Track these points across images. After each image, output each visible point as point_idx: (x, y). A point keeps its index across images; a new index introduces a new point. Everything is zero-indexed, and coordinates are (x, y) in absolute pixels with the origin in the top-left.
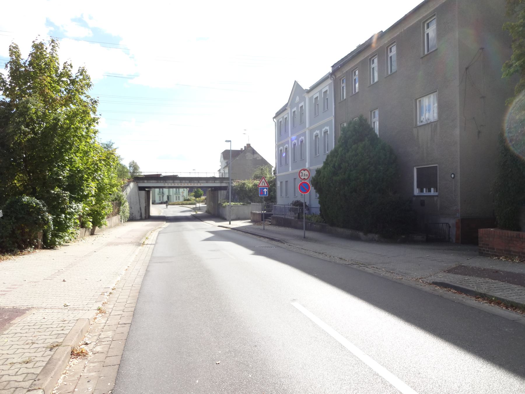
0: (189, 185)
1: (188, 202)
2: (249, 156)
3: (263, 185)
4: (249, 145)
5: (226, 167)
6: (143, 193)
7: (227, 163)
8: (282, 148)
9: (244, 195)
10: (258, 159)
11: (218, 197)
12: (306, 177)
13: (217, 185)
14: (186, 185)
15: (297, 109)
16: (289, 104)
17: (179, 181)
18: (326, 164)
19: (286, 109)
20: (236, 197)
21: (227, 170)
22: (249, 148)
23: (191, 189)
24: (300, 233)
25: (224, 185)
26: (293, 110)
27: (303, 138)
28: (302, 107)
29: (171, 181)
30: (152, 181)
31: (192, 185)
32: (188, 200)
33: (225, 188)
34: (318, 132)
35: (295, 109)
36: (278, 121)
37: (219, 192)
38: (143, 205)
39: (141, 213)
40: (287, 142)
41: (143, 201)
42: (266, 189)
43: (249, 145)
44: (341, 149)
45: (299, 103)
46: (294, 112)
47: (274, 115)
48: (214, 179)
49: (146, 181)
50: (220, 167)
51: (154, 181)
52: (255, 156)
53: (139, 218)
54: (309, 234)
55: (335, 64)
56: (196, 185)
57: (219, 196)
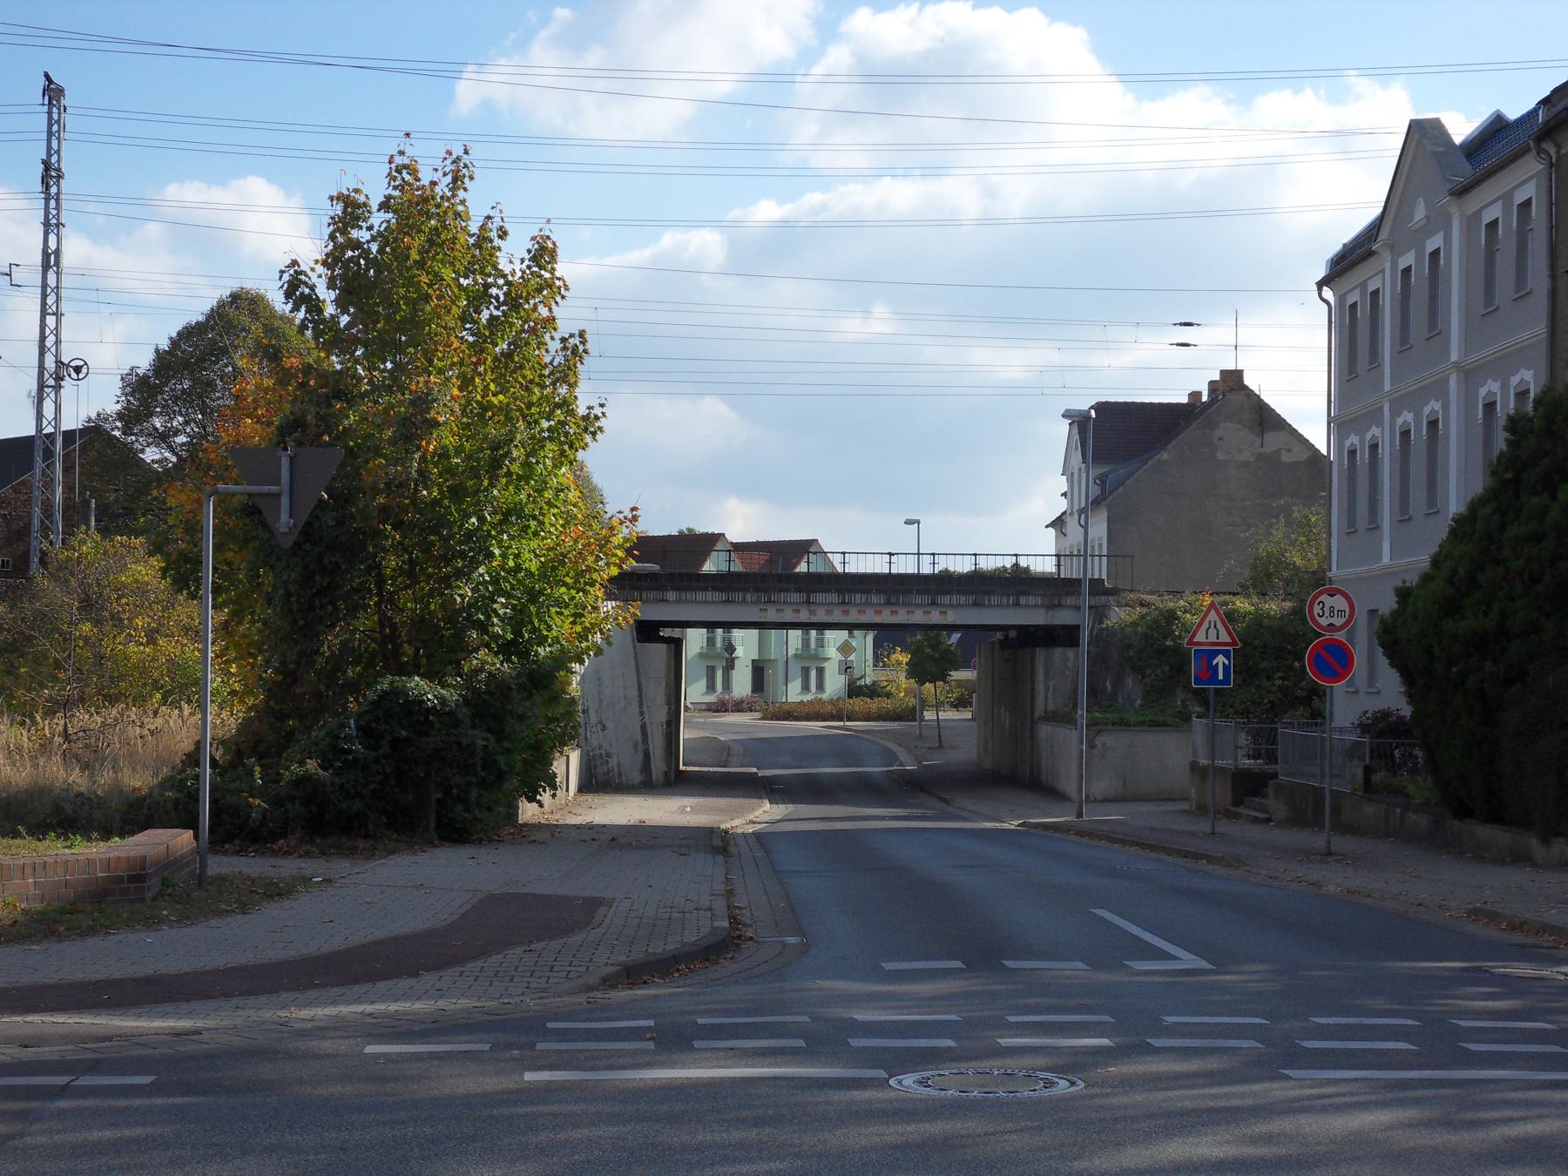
0: (887, 617)
1: (874, 705)
2: (1234, 441)
3: (1213, 639)
4: (1231, 381)
5: (1096, 503)
6: (659, 651)
7: (1102, 480)
8: (1408, 417)
9: (1153, 671)
10: (1286, 458)
11: (1033, 681)
12: (1338, 622)
13: (1034, 616)
14: (869, 617)
15: (1419, 258)
16: (1384, 234)
17: (833, 597)
18: (1435, 562)
19: (1371, 253)
20: (1129, 681)
21: (1099, 529)
22: (1236, 398)
23: (887, 636)
24: (1318, 840)
25: (1063, 618)
26: (1402, 264)
27: (1436, 405)
28: (1436, 253)
29: (796, 597)
30: (700, 596)
31: (902, 617)
32: (873, 691)
33: (1068, 636)
34: (1493, 386)
35: (1408, 260)
36: (1341, 299)
37: (1041, 654)
38: (659, 714)
39: (647, 755)
40: (1438, 389)
41: (657, 694)
42: (1226, 654)
43: (1231, 381)
44: (1488, 510)
45: (1425, 231)
46: (1407, 271)
47: (1321, 273)
48: (1016, 582)
49: (671, 595)
50: (1062, 505)
51: (710, 596)
52: (1273, 440)
53: (636, 777)
54: (1341, 843)
55: (1556, 91)
56: (919, 617)
57: (1040, 676)
